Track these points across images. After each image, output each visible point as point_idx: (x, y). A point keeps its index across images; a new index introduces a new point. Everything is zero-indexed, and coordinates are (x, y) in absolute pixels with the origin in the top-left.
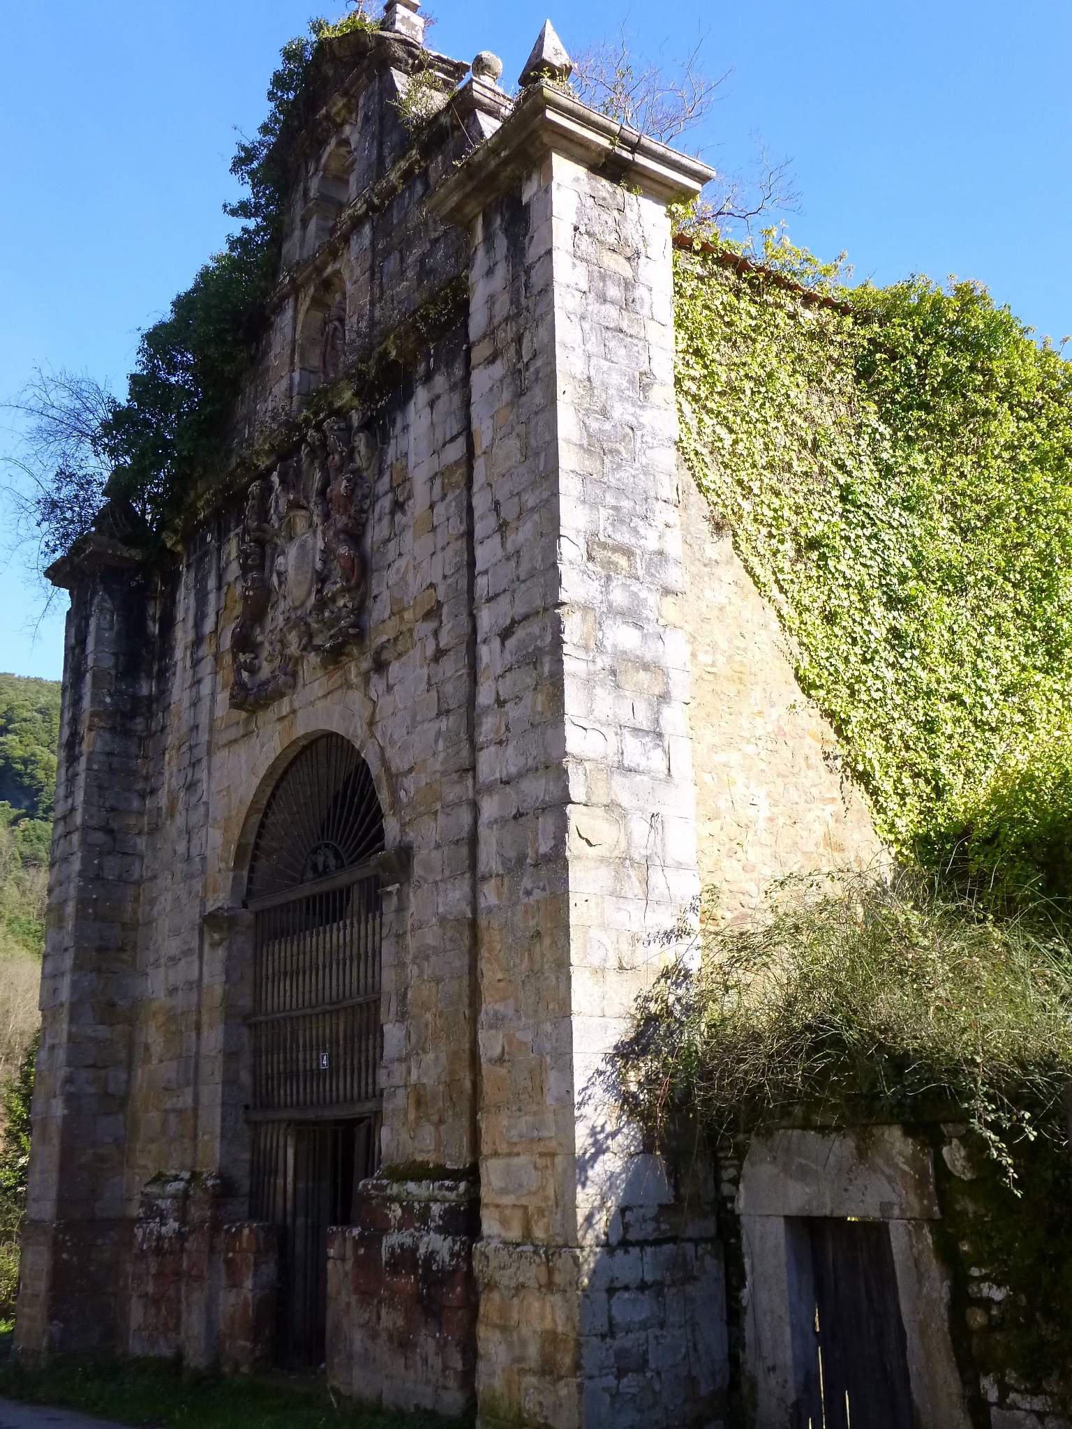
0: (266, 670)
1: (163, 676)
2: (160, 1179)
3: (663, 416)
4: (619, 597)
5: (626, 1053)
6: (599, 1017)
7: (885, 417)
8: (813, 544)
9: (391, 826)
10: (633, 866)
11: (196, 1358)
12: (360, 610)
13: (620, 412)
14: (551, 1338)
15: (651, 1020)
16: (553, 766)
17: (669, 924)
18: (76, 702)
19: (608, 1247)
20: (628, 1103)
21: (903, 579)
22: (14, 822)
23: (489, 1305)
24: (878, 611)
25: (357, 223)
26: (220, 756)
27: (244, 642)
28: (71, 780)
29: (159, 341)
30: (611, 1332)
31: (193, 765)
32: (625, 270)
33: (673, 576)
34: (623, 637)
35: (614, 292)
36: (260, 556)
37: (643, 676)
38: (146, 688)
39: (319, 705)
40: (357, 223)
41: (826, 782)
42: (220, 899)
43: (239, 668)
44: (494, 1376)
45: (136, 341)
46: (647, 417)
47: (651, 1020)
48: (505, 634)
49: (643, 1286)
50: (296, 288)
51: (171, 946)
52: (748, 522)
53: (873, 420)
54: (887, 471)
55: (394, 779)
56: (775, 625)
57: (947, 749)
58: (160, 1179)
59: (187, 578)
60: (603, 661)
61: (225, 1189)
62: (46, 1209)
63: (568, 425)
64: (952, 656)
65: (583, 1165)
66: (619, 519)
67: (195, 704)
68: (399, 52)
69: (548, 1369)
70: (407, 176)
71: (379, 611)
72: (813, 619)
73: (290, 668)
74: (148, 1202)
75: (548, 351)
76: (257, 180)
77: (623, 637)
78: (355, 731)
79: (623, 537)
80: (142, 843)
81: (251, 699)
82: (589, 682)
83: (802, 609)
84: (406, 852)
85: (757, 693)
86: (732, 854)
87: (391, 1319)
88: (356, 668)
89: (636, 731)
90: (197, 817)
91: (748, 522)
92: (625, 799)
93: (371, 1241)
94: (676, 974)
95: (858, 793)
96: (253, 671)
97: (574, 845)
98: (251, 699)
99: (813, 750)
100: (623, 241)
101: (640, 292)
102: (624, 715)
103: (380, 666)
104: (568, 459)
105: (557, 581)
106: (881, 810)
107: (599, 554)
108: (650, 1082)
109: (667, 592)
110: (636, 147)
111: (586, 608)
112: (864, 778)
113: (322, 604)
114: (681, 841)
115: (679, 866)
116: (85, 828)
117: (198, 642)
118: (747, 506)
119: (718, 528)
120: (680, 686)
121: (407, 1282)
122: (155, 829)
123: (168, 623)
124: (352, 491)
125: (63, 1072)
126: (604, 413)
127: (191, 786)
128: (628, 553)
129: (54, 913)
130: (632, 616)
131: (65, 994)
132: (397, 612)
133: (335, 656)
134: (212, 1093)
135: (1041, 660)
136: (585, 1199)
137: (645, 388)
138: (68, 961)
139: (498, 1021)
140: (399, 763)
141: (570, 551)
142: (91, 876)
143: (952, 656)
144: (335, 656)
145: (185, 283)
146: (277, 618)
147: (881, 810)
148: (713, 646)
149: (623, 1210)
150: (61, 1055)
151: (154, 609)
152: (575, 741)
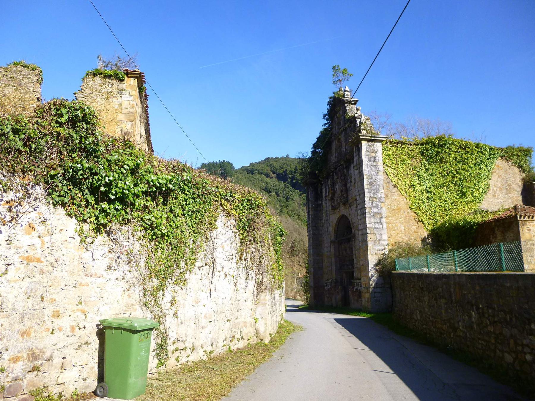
0: (336, 204)
1: (322, 200)
2: (328, 280)
3: (381, 177)
4: (374, 205)
5: (376, 265)
6: (372, 260)
7: (427, 160)
8: (412, 185)
9: (353, 230)
10: (377, 241)
11: (334, 305)
12: (347, 197)
13: (373, 178)
14: (368, 298)
15: (380, 260)
16: (365, 228)
17: (383, 248)
18: (309, 205)
19: (374, 287)
20: (377, 271)
21: (430, 188)
22: (300, 195)
23: (363, 295)
24: (424, 194)
25: (342, 132)
26: (331, 216)
27: (332, 199)
28: (309, 218)
29: (315, 146)
30: (375, 297)
31: (327, 217)
32: (374, 155)
33: (383, 200)
34: (376, 210)
35: (372, 159)
36: (333, 184)
37: (378, 215)
38: (319, 202)
39: (343, 211)
40: (342, 132)
41: (414, 223)
42: (332, 238)
43: (332, 203)
44: (363, 303)
45: (311, 146)
46: (378, 177)
47: (380, 260)
48: (360, 210)
49: (379, 292)
50: (335, 139)
51: (326, 245)
52: (400, 185)
53: (425, 162)
54: (427, 170)
55: (353, 223)
56: (405, 200)
57: (438, 214)
58: (328, 280)
59: (324, 185)
60: (372, 214)
61: (336, 282)
62: (312, 284)
63: (366, 182)
64: (440, 198)
65: (370, 279)
66: (374, 193)
67: (327, 207)
68: (346, 101)
69: (368, 302)
70: (348, 126)
71: (350, 197)
72: (412, 198)
73: (339, 204)
74: (326, 283)
75: (362, 171)
76: (327, 119)
77: (376, 210)
78: (348, 215)
79: (375, 196)
80: (321, 228)
81: (334, 208)
82: (370, 218)
83: (410, 196)
84: (355, 235)
85: (402, 211)
86: (397, 235)
87: (355, 298)
88: (347, 206)
89: (377, 223)
90: (328, 225)
91: (400, 185)
92: (376, 232)
93: (353, 288)
94: (384, 254)
95: (421, 224)
96: (334, 203)
97: (368, 239)
98: (334, 208)
99: (412, 218)
100: (374, 150)
101: (377, 158)
102: (375, 221)
103: (350, 206)
104: (366, 187)
105: (365, 204)
106: (425, 226)
107: (371, 199)
108: (380, 268)
109: (382, 202)
110: (374, 137)
111: (369, 207)
112: (422, 221)
113: (342, 195)
114: (385, 237)
115: (384, 240)
116: (312, 226)
117: (326, 197)
118: (400, 182)
119: (395, 186)
120: (384, 215)
121: (357, 293)
122: (323, 226)
123: (322, 192)
124: (344, 178)
125: (312, 264)
126: (371, 178)
127: (327, 220)
128: (376, 198)
129: (308, 263)
130: (376, 207)
131: (312, 252)
132: (352, 198)
133: (344, 204)
134: (334, 268)
135: (460, 196)
136: (371, 283)
137: (378, 173)
138: (312, 247)
139: (362, 260)
140: (354, 221)
141: (367, 199)
142: (314, 234)
143: (440, 198)
144: (344, 204)
145: (318, 135)
146: (336, 195)
147: (425, 226)
148: (394, 205)
149: (376, 283)
150: (312, 261)
151: (319, 189)
152: (368, 225)
